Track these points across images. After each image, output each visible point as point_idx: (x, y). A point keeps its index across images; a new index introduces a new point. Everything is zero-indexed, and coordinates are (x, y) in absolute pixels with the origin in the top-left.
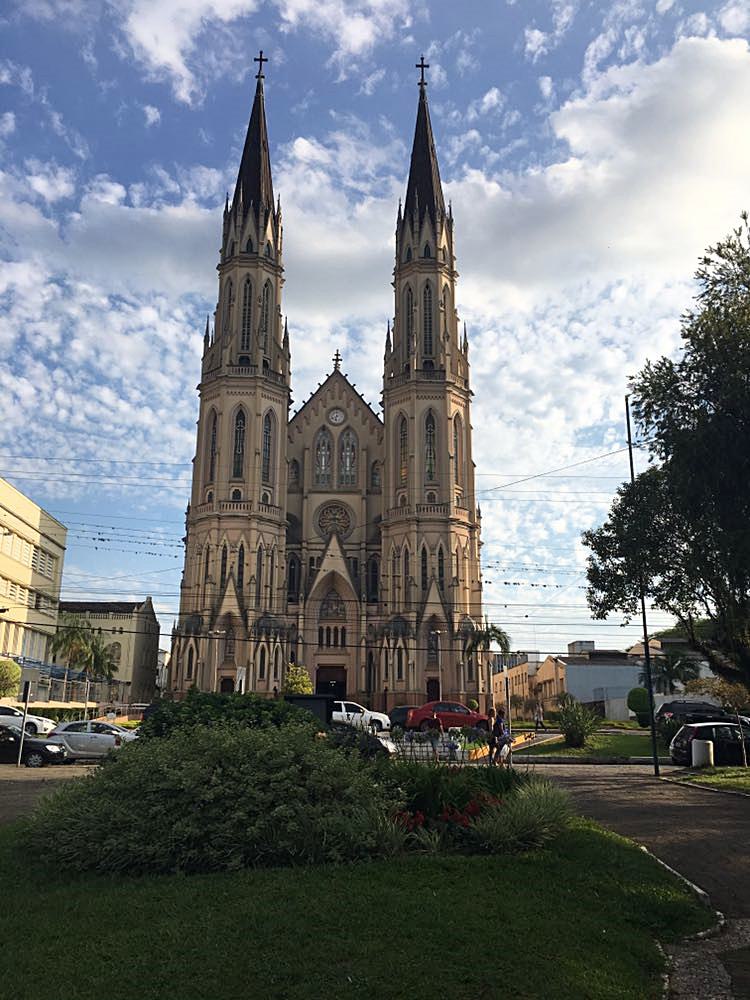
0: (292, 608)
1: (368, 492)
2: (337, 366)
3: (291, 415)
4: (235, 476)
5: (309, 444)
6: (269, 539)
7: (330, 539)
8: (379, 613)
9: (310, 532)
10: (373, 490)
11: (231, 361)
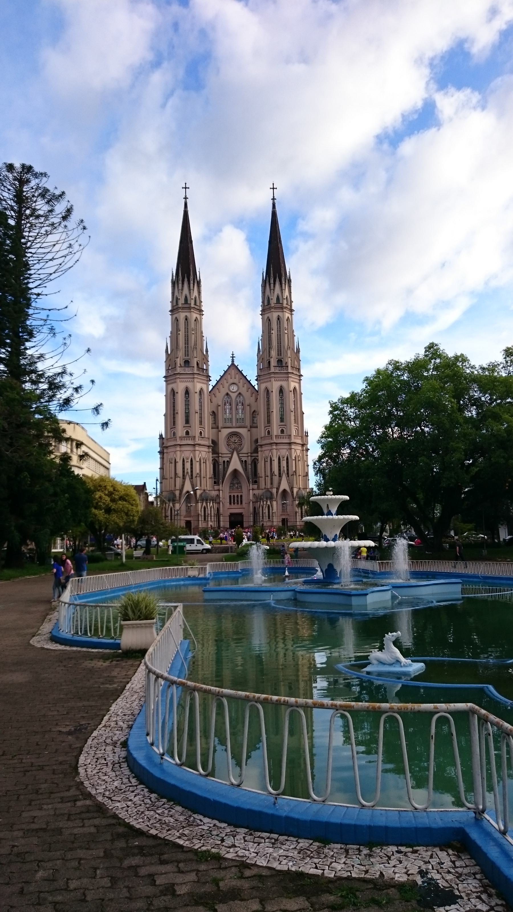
0: (216, 487)
1: (251, 427)
2: (233, 361)
3: (211, 388)
4: (186, 423)
5: (220, 403)
6: (204, 455)
7: (232, 454)
8: (258, 488)
9: (223, 448)
10: (253, 426)
11: (180, 364)
